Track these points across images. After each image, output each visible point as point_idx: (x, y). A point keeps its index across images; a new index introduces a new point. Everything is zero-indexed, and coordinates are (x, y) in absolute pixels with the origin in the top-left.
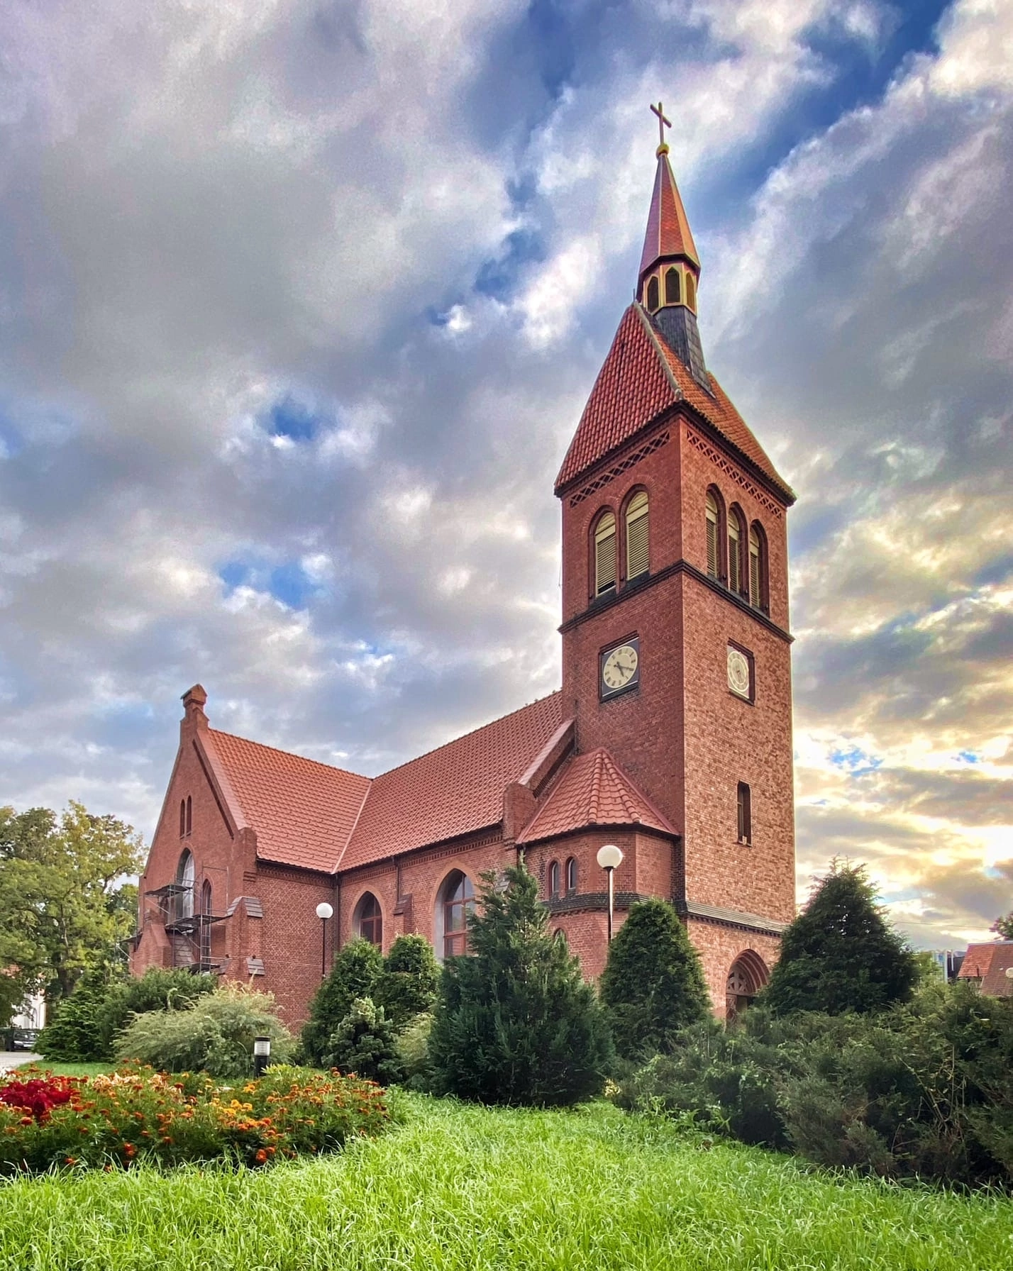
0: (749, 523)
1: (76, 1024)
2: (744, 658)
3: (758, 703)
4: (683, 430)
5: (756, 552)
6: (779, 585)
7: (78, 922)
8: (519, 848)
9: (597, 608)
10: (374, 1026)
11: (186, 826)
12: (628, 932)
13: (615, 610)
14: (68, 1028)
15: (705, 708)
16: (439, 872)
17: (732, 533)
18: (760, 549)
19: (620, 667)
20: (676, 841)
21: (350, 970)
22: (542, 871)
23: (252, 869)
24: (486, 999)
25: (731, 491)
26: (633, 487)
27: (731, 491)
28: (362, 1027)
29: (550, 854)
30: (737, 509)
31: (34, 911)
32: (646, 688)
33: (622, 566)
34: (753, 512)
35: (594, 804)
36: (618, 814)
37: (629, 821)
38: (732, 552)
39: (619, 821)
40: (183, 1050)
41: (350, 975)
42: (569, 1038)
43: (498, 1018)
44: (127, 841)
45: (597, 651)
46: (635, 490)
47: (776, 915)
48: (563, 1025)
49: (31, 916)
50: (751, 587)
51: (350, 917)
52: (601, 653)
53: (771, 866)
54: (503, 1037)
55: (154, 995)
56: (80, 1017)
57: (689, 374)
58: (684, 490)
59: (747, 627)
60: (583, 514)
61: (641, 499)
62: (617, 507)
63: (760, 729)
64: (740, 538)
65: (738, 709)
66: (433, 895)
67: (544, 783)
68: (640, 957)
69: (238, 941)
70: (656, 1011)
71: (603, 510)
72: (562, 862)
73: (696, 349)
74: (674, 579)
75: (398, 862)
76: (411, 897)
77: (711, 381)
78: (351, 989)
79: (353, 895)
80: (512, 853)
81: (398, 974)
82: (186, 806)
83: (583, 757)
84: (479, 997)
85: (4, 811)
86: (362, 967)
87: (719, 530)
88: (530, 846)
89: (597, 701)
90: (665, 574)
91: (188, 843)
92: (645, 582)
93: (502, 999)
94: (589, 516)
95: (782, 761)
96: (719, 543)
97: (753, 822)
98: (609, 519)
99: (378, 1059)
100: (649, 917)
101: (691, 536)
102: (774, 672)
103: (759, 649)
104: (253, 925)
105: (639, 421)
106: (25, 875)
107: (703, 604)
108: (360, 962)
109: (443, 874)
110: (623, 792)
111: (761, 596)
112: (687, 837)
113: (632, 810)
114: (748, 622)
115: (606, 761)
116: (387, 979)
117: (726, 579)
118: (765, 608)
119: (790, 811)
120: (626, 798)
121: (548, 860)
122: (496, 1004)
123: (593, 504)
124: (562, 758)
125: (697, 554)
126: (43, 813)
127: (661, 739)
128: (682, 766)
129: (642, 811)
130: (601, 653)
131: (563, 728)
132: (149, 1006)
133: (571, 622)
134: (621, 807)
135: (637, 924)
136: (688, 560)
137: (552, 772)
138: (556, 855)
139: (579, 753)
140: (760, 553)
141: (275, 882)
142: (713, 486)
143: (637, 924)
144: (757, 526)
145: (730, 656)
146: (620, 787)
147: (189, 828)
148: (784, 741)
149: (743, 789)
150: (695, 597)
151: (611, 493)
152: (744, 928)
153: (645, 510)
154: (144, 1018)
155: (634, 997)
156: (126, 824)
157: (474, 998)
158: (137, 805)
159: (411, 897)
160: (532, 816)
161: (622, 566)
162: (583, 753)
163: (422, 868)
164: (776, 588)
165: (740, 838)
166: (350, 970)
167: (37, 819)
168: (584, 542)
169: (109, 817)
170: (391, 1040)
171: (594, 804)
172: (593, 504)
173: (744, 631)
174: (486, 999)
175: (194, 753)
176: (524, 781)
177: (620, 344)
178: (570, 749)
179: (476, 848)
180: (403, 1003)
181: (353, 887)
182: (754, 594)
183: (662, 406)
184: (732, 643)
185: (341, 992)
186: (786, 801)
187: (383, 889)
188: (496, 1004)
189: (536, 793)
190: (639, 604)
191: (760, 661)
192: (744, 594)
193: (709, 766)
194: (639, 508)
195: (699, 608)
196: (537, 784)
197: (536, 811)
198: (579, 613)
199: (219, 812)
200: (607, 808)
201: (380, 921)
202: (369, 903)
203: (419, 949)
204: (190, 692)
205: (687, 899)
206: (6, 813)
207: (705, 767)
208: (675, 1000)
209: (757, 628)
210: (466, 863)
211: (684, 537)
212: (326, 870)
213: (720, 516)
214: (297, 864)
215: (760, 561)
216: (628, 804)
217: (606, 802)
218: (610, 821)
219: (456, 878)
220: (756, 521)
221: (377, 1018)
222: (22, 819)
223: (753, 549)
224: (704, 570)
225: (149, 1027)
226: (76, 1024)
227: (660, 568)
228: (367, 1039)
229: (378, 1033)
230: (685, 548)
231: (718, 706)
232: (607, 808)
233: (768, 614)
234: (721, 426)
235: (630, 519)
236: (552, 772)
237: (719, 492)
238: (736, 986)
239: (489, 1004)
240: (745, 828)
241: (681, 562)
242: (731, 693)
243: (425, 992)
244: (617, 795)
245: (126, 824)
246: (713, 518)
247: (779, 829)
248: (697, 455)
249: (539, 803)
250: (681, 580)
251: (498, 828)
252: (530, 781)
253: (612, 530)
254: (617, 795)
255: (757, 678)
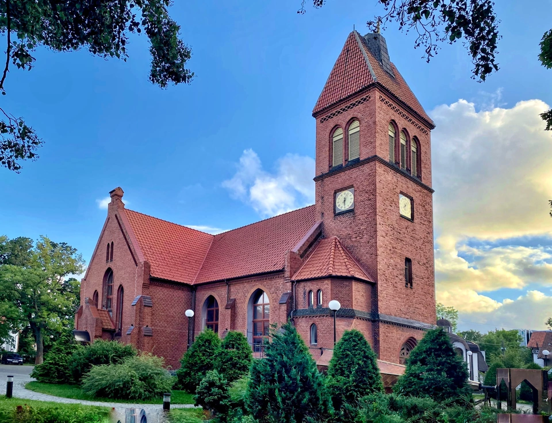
0: (411, 137)
1: (56, 364)
2: (408, 201)
3: (415, 221)
4: (377, 94)
5: (415, 150)
6: (427, 166)
7: (44, 298)
8: (293, 282)
9: (334, 171)
10: (218, 383)
11: (110, 256)
12: (342, 344)
13: (342, 174)
14: (51, 366)
15: (387, 224)
16: (250, 288)
17: (402, 141)
18: (417, 149)
19: (346, 200)
20: (373, 286)
21: (203, 345)
22: (305, 294)
23: (147, 282)
24: (272, 381)
25: (402, 123)
26: (352, 118)
27: (402, 123)
28: (212, 384)
29: (309, 286)
30: (405, 131)
31: (17, 290)
32: (358, 212)
33: (346, 154)
34: (413, 131)
35: (331, 265)
36: (344, 271)
37: (349, 275)
38: (403, 151)
39: (344, 275)
40: (118, 385)
41: (203, 348)
42: (310, 400)
43: (277, 391)
44: (73, 257)
45: (333, 192)
46: (353, 120)
47: (426, 320)
48: (307, 396)
49: (16, 293)
50: (412, 166)
51: (202, 303)
52: (335, 193)
53: (424, 297)
54: (279, 399)
55: (100, 355)
56: (58, 361)
57: (381, 67)
58: (378, 123)
59: (410, 186)
60: (327, 127)
61: (356, 123)
62: (344, 126)
63: (417, 233)
64: (407, 144)
65: (405, 223)
66: (247, 300)
67: (306, 251)
68: (347, 355)
69: (138, 318)
70: (354, 381)
71: (336, 127)
72: (315, 291)
73: (385, 54)
74: (372, 164)
75: (229, 282)
76: (235, 300)
77: (393, 68)
78: (204, 355)
79: (203, 296)
80: (289, 284)
81: (229, 350)
82: (110, 247)
83: (326, 240)
84: (269, 380)
85: (1, 238)
86: (210, 344)
87: (395, 141)
88: (299, 281)
89: (333, 215)
90: (368, 160)
91: (110, 265)
92: (357, 163)
93: (280, 382)
94: (330, 128)
95: (428, 247)
96: (395, 146)
97: (414, 276)
98: (340, 131)
99: (220, 399)
100: (352, 337)
101: (381, 144)
102: (424, 206)
103: (417, 196)
104: (147, 310)
105: (355, 88)
106: (14, 274)
107: (387, 176)
108: (209, 341)
109: (253, 290)
110: (346, 260)
111: (417, 170)
112: (379, 283)
113: (350, 269)
114: (411, 184)
115: (338, 243)
116: (223, 352)
117: (399, 163)
118: (419, 176)
119: (433, 272)
120: (347, 263)
121: (308, 289)
122: (277, 384)
123: (331, 124)
124: (316, 239)
125: (385, 154)
126: (25, 239)
127: (365, 236)
128: (376, 250)
129: (356, 270)
130: (335, 193)
131: (316, 226)
132: (98, 362)
133: (320, 177)
134: (345, 267)
135: (346, 340)
136: (378, 154)
137: (310, 246)
138: (312, 288)
139: (324, 238)
140: (417, 151)
141: (159, 288)
142: (393, 120)
143: (346, 340)
144: (416, 139)
145: (401, 199)
146: (345, 257)
147: (112, 257)
148: (430, 239)
149: (408, 261)
150: (383, 172)
151: (343, 119)
152: (409, 327)
153: (358, 129)
154: (96, 369)
155: (344, 374)
156: (73, 248)
157: (266, 381)
158: (85, 248)
159: (235, 300)
160: (300, 267)
161: (346, 154)
162: (326, 238)
163: (241, 286)
164: (425, 167)
165: (407, 284)
166: (203, 345)
167: (21, 244)
168: (327, 140)
169: (64, 243)
170: (226, 390)
171: (331, 265)
172: (331, 124)
173: (408, 188)
174: (272, 381)
175: (116, 221)
176: (295, 250)
177: (347, 50)
178: (319, 236)
179: (271, 279)
180: (233, 368)
181: (203, 292)
182: (414, 169)
183: (367, 83)
184: (402, 193)
185: (199, 356)
186: (431, 266)
187: (220, 295)
188: (277, 384)
189: (302, 256)
190: (355, 173)
191: (417, 201)
192: (409, 170)
193: (390, 250)
194: (355, 127)
195: (385, 178)
196: (302, 252)
197: (301, 264)
198: (324, 173)
199: (129, 252)
200: (338, 267)
201: (217, 311)
202: (211, 302)
203: (240, 338)
204: (114, 191)
205: (379, 313)
206: (2, 239)
207: (388, 251)
208: (364, 376)
209: (415, 186)
210: (265, 286)
211: (377, 145)
212: (188, 283)
213: (396, 134)
214: (173, 280)
215: (417, 155)
216: (349, 266)
217: (337, 264)
218: (339, 274)
219: (258, 293)
220: (415, 136)
221: (220, 379)
222: (11, 242)
223: (413, 149)
224: (387, 160)
225: (98, 373)
226: (56, 364)
227: (366, 157)
228: (215, 390)
229: (220, 387)
230: (378, 149)
231: (394, 223)
232: (338, 267)
233: (421, 180)
234: (398, 93)
235: (350, 132)
236: (310, 246)
237: (396, 124)
238: (405, 354)
239: (274, 384)
240: (409, 280)
241: (376, 156)
242: (402, 216)
243: (243, 360)
244: (343, 261)
245: (73, 248)
246: (393, 135)
247: (427, 280)
248: (385, 107)
249: (303, 261)
250: (375, 164)
251: (282, 271)
252: (299, 250)
253: (341, 136)
254: (343, 261)
255: (415, 209)
